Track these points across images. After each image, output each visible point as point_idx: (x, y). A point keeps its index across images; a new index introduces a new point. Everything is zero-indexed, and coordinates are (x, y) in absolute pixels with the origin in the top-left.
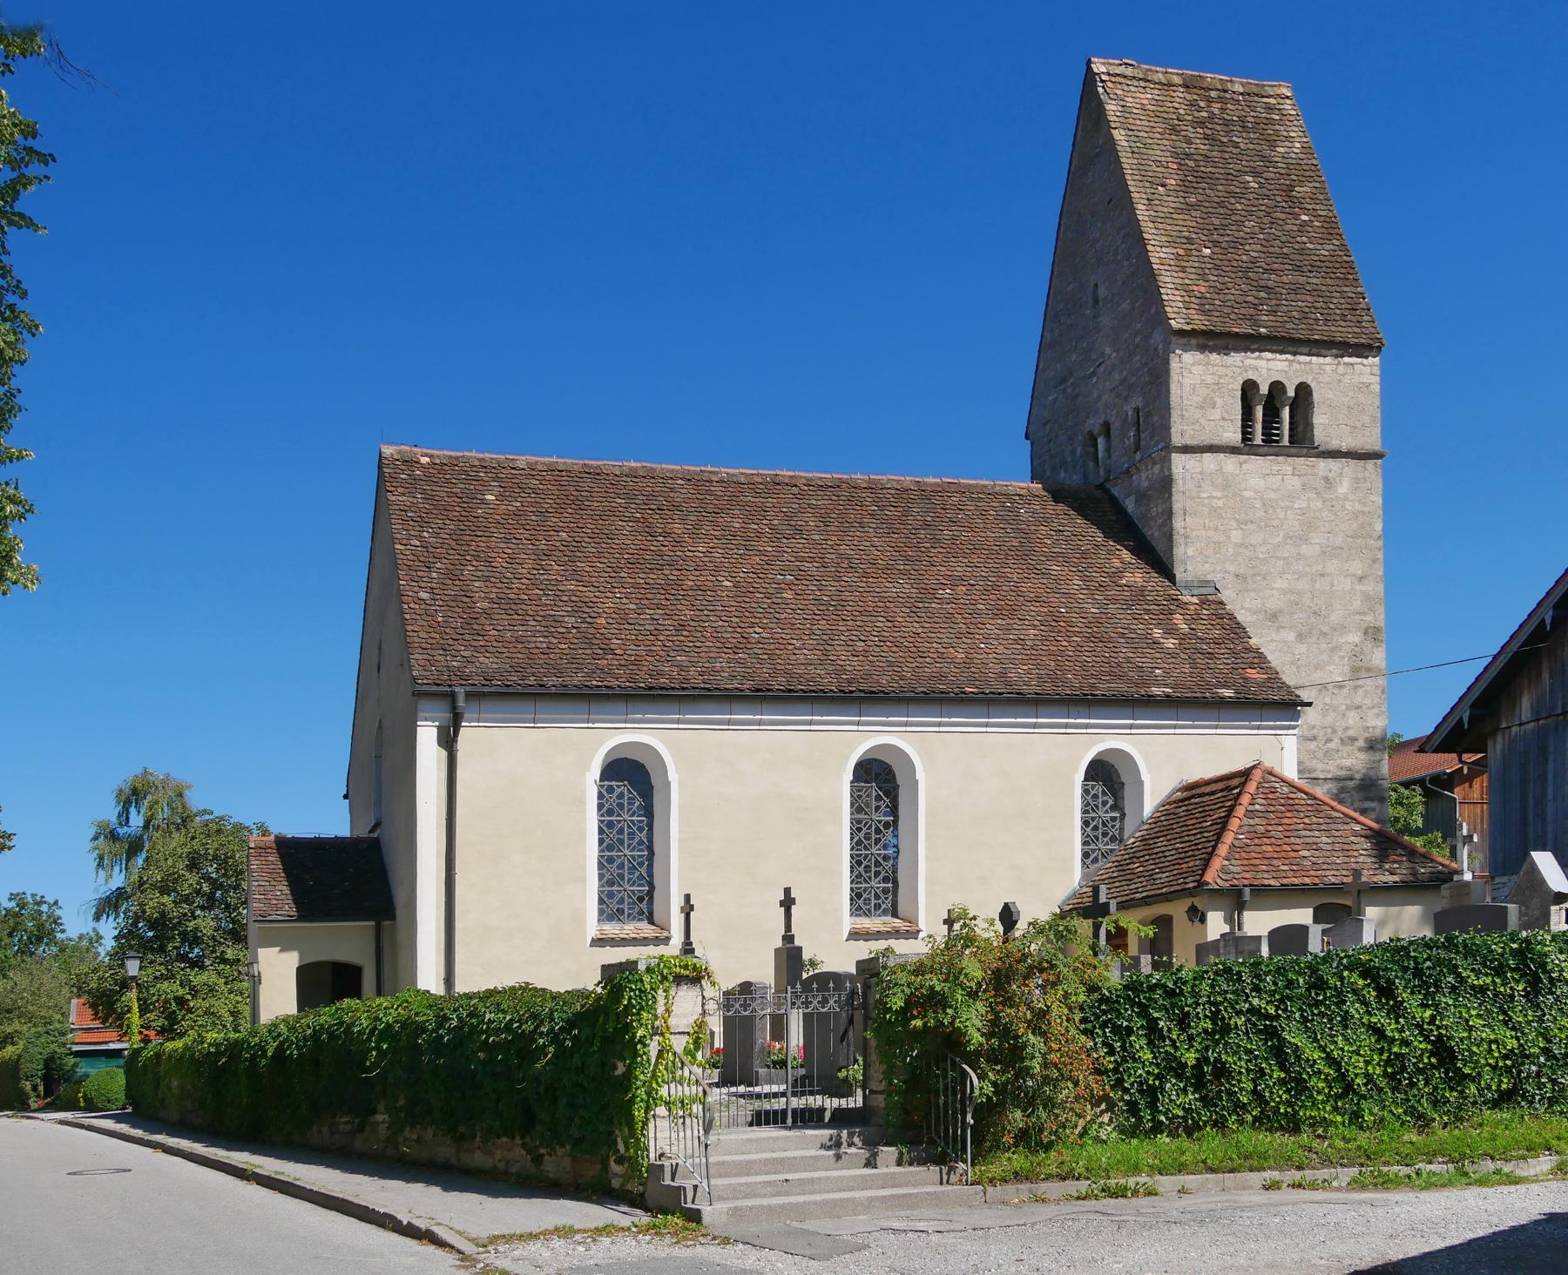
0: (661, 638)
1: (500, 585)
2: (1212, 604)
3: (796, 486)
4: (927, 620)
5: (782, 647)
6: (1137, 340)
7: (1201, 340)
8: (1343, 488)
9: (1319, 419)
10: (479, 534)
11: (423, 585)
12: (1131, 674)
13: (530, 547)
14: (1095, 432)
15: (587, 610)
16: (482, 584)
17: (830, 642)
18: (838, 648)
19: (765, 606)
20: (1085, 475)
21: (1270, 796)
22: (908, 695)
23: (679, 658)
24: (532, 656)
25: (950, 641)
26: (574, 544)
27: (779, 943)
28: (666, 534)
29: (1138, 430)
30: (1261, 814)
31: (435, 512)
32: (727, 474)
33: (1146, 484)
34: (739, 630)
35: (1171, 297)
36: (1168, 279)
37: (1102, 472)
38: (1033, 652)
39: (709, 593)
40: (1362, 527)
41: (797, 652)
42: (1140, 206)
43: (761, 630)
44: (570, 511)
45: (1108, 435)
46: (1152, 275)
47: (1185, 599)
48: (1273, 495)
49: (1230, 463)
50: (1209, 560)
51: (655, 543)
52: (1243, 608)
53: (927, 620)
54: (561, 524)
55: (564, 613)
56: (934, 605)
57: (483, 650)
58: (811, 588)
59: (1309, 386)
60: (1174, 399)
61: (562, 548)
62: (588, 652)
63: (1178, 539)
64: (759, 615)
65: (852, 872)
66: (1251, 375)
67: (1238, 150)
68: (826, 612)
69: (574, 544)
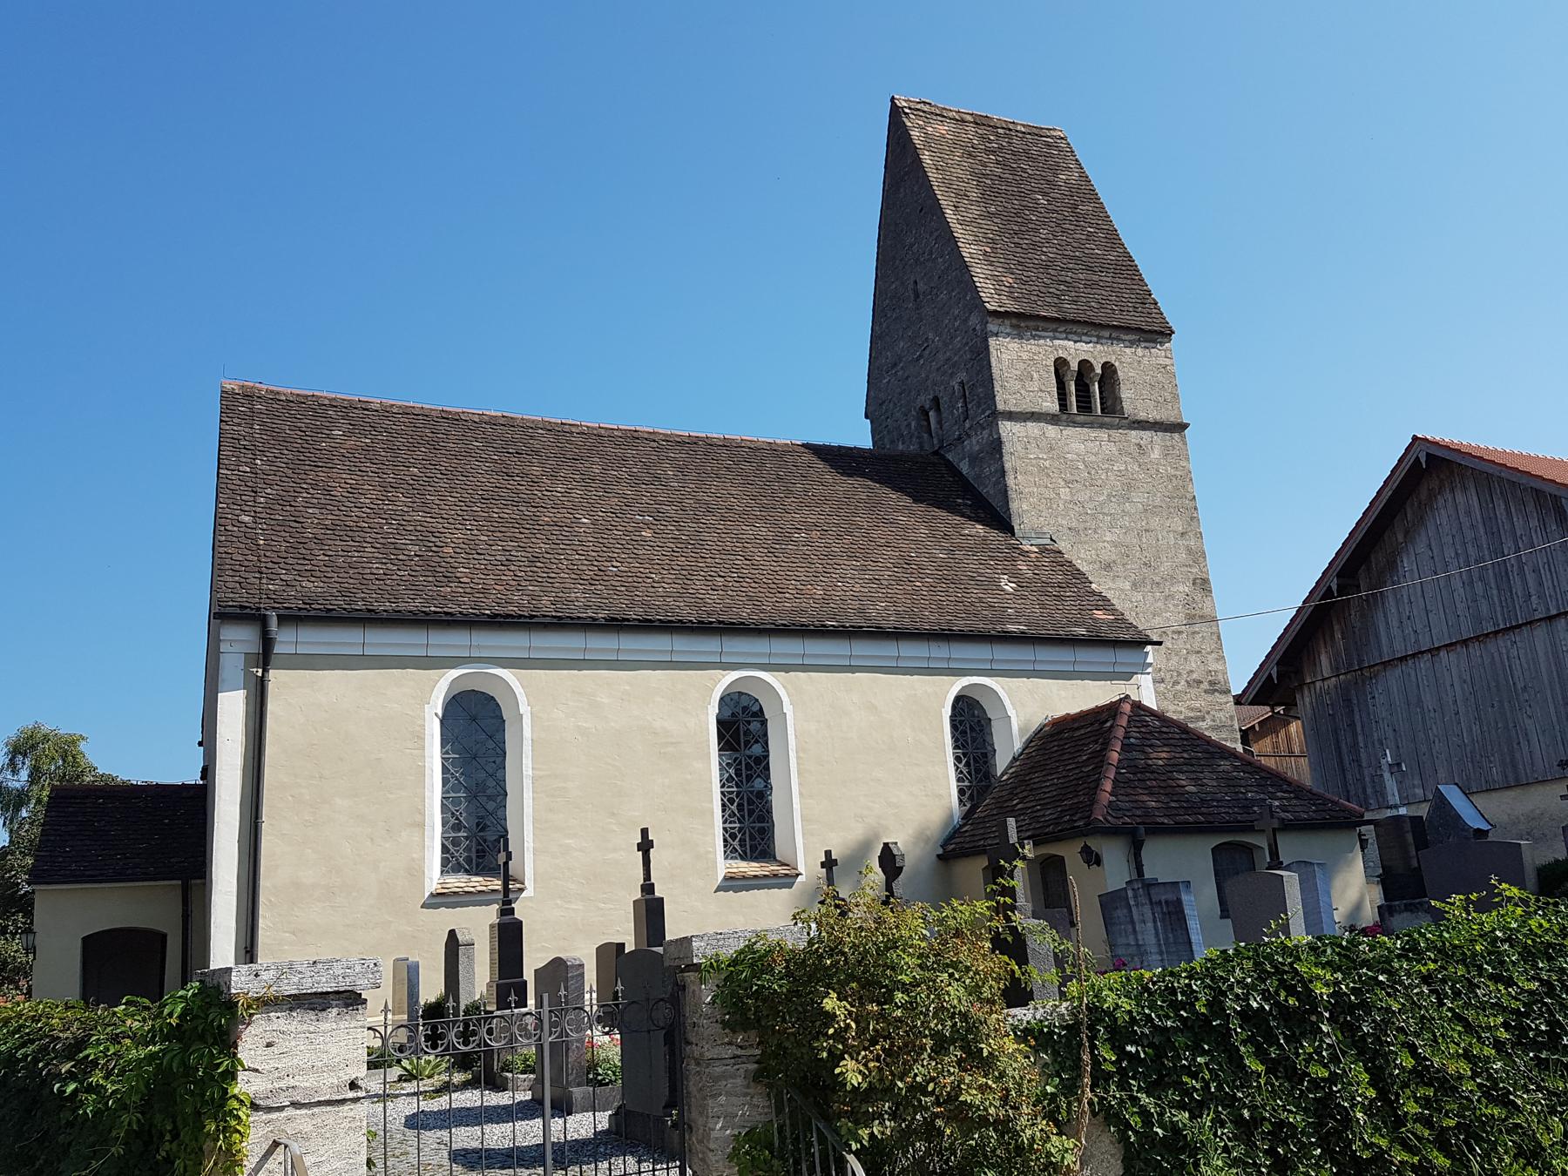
0: (513, 568)
1: (337, 513)
2: (1050, 552)
3: (654, 441)
4: (786, 560)
5: (640, 580)
6: (957, 324)
7: (1014, 321)
8: (1156, 454)
9: (1126, 394)
10: (320, 464)
11: (247, 508)
12: (984, 612)
13: (377, 479)
14: (927, 407)
15: (433, 539)
16: (317, 511)
17: (689, 577)
18: (697, 583)
19: (624, 542)
20: (921, 447)
21: (1142, 730)
22: (768, 626)
23: (531, 588)
24: (365, 582)
25: (808, 579)
26: (425, 479)
27: (638, 895)
28: (524, 475)
29: (965, 403)
30: (1138, 748)
31: (272, 442)
32: (587, 427)
33: (977, 448)
34: (596, 563)
35: (984, 285)
36: (979, 271)
37: (935, 441)
38: (889, 591)
39: (566, 529)
40: (1176, 488)
41: (656, 585)
42: (948, 211)
43: (619, 564)
44: (424, 450)
45: (938, 410)
46: (965, 267)
47: (1027, 548)
48: (1093, 458)
49: (1052, 431)
50: (1043, 514)
51: (511, 482)
52: (1079, 558)
53: (786, 560)
54: (412, 461)
55: (408, 542)
56: (790, 547)
57: (309, 574)
58: (670, 527)
59: (1113, 365)
60: (995, 371)
61: (411, 482)
62: (430, 579)
63: (1012, 495)
64: (617, 551)
65: (723, 811)
66: (1061, 354)
67: (1026, 175)
68: (685, 550)
69: (425, 479)
